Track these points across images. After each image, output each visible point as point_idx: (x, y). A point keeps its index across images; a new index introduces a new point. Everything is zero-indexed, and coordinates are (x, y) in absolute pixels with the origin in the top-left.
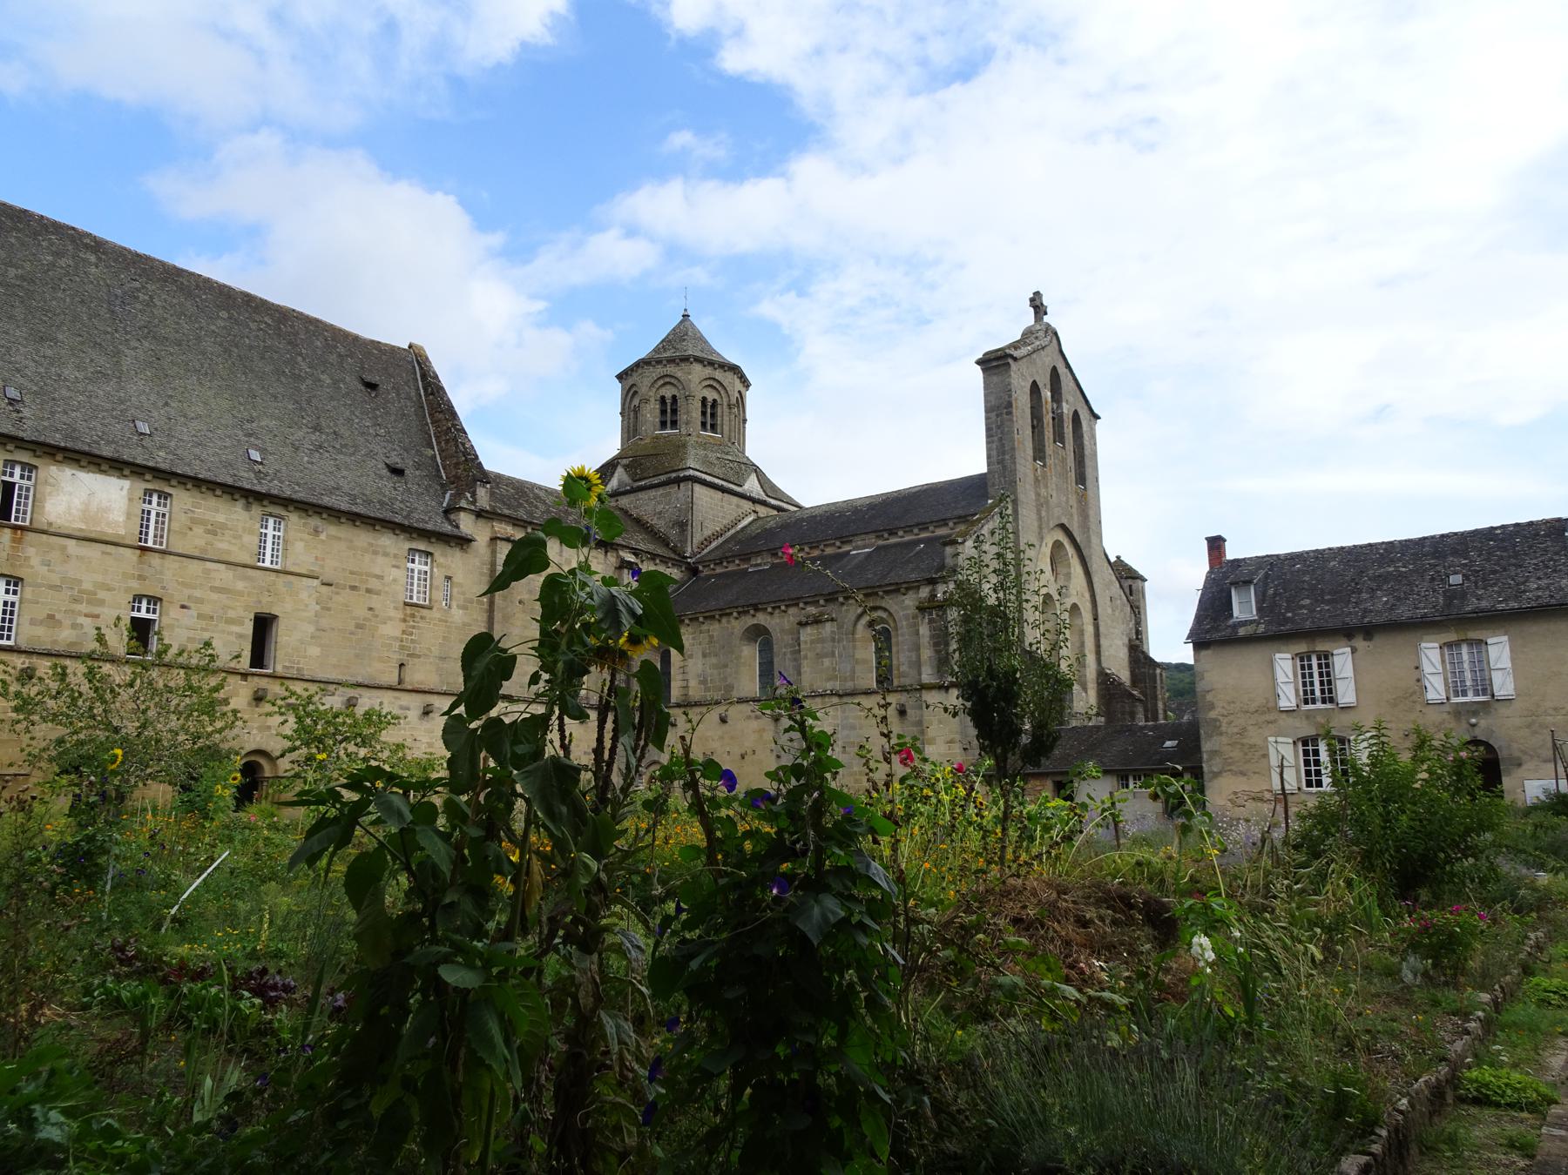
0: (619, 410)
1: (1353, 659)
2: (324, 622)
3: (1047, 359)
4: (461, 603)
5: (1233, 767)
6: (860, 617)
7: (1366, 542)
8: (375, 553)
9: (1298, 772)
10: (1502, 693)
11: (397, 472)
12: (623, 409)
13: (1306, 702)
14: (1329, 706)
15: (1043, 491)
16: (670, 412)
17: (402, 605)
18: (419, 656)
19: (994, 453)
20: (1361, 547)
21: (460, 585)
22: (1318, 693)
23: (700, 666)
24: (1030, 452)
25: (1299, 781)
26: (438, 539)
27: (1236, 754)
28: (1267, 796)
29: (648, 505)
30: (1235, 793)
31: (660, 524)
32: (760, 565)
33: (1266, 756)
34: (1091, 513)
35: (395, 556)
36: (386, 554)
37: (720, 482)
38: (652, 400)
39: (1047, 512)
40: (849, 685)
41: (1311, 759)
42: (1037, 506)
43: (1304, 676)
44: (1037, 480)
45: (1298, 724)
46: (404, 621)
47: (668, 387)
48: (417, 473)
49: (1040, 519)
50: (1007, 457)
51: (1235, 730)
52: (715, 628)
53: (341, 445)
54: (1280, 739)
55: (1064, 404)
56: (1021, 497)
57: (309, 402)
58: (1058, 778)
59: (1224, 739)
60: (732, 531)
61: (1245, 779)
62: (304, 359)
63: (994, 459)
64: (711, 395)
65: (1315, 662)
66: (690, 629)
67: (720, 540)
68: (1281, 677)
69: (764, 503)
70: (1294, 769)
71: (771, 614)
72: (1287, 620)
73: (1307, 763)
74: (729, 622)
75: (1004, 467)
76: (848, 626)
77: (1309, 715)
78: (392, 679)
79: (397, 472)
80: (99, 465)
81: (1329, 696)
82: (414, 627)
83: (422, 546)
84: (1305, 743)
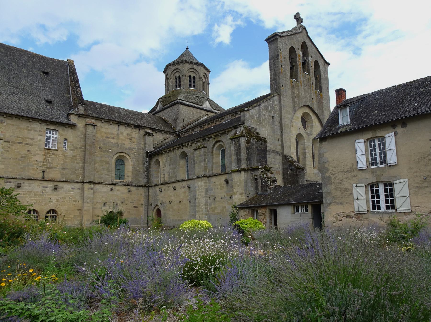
0: (388, 87)
1: (395, 139)
2: (6, 156)
3: (301, 38)
4: (72, 148)
5: (336, 200)
6: (214, 145)
7: (413, 80)
8: (30, 130)
9: (367, 202)
10: (391, 162)
11: (49, 102)
12: (166, 83)
13: (372, 165)
14: (384, 165)
15: (296, 91)
16: (178, 82)
17: (43, 149)
18: (52, 168)
19: (273, 76)
20: (410, 83)
21: (71, 142)
22: (378, 159)
23: (168, 169)
24: (289, 75)
25: (368, 206)
26: (59, 125)
27: (338, 194)
28: (353, 215)
29: (167, 115)
30: (337, 214)
31: (169, 120)
32: (196, 131)
33: (352, 194)
34: (324, 102)
35: (40, 131)
36: (35, 131)
37: (192, 104)
38: (172, 78)
39: (299, 100)
40: (211, 173)
41: (375, 194)
42: (292, 97)
43: (371, 151)
44: (292, 86)
45: (367, 177)
46: (45, 155)
47: (178, 73)
48: (60, 102)
49: (294, 102)
50: (277, 77)
51: (338, 181)
52: (172, 154)
53: (25, 93)
54: (358, 185)
55: (310, 57)
56: (283, 93)
57: (14, 78)
58: (271, 208)
59: (333, 186)
60: (198, 122)
61: (342, 206)
62: (16, 63)
63: (273, 79)
64: (192, 75)
65: (377, 143)
66: (165, 155)
67: (192, 125)
68: (359, 152)
69: (212, 112)
70: (365, 201)
71: (187, 147)
72: (363, 122)
73: (373, 197)
74: (176, 152)
75: (276, 81)
76: (210, 149)
77: (373, 172)
78: (40, 176)
79: (49, 102)
80: (12, 117)
81: (384, 161)
82: (49, 157)
83: (53, 127)
84: (372, 187)
